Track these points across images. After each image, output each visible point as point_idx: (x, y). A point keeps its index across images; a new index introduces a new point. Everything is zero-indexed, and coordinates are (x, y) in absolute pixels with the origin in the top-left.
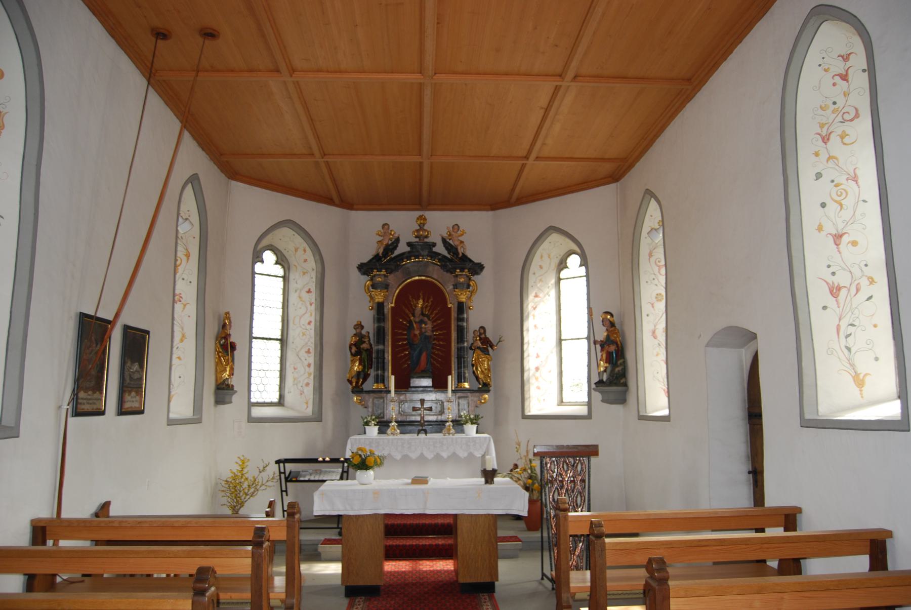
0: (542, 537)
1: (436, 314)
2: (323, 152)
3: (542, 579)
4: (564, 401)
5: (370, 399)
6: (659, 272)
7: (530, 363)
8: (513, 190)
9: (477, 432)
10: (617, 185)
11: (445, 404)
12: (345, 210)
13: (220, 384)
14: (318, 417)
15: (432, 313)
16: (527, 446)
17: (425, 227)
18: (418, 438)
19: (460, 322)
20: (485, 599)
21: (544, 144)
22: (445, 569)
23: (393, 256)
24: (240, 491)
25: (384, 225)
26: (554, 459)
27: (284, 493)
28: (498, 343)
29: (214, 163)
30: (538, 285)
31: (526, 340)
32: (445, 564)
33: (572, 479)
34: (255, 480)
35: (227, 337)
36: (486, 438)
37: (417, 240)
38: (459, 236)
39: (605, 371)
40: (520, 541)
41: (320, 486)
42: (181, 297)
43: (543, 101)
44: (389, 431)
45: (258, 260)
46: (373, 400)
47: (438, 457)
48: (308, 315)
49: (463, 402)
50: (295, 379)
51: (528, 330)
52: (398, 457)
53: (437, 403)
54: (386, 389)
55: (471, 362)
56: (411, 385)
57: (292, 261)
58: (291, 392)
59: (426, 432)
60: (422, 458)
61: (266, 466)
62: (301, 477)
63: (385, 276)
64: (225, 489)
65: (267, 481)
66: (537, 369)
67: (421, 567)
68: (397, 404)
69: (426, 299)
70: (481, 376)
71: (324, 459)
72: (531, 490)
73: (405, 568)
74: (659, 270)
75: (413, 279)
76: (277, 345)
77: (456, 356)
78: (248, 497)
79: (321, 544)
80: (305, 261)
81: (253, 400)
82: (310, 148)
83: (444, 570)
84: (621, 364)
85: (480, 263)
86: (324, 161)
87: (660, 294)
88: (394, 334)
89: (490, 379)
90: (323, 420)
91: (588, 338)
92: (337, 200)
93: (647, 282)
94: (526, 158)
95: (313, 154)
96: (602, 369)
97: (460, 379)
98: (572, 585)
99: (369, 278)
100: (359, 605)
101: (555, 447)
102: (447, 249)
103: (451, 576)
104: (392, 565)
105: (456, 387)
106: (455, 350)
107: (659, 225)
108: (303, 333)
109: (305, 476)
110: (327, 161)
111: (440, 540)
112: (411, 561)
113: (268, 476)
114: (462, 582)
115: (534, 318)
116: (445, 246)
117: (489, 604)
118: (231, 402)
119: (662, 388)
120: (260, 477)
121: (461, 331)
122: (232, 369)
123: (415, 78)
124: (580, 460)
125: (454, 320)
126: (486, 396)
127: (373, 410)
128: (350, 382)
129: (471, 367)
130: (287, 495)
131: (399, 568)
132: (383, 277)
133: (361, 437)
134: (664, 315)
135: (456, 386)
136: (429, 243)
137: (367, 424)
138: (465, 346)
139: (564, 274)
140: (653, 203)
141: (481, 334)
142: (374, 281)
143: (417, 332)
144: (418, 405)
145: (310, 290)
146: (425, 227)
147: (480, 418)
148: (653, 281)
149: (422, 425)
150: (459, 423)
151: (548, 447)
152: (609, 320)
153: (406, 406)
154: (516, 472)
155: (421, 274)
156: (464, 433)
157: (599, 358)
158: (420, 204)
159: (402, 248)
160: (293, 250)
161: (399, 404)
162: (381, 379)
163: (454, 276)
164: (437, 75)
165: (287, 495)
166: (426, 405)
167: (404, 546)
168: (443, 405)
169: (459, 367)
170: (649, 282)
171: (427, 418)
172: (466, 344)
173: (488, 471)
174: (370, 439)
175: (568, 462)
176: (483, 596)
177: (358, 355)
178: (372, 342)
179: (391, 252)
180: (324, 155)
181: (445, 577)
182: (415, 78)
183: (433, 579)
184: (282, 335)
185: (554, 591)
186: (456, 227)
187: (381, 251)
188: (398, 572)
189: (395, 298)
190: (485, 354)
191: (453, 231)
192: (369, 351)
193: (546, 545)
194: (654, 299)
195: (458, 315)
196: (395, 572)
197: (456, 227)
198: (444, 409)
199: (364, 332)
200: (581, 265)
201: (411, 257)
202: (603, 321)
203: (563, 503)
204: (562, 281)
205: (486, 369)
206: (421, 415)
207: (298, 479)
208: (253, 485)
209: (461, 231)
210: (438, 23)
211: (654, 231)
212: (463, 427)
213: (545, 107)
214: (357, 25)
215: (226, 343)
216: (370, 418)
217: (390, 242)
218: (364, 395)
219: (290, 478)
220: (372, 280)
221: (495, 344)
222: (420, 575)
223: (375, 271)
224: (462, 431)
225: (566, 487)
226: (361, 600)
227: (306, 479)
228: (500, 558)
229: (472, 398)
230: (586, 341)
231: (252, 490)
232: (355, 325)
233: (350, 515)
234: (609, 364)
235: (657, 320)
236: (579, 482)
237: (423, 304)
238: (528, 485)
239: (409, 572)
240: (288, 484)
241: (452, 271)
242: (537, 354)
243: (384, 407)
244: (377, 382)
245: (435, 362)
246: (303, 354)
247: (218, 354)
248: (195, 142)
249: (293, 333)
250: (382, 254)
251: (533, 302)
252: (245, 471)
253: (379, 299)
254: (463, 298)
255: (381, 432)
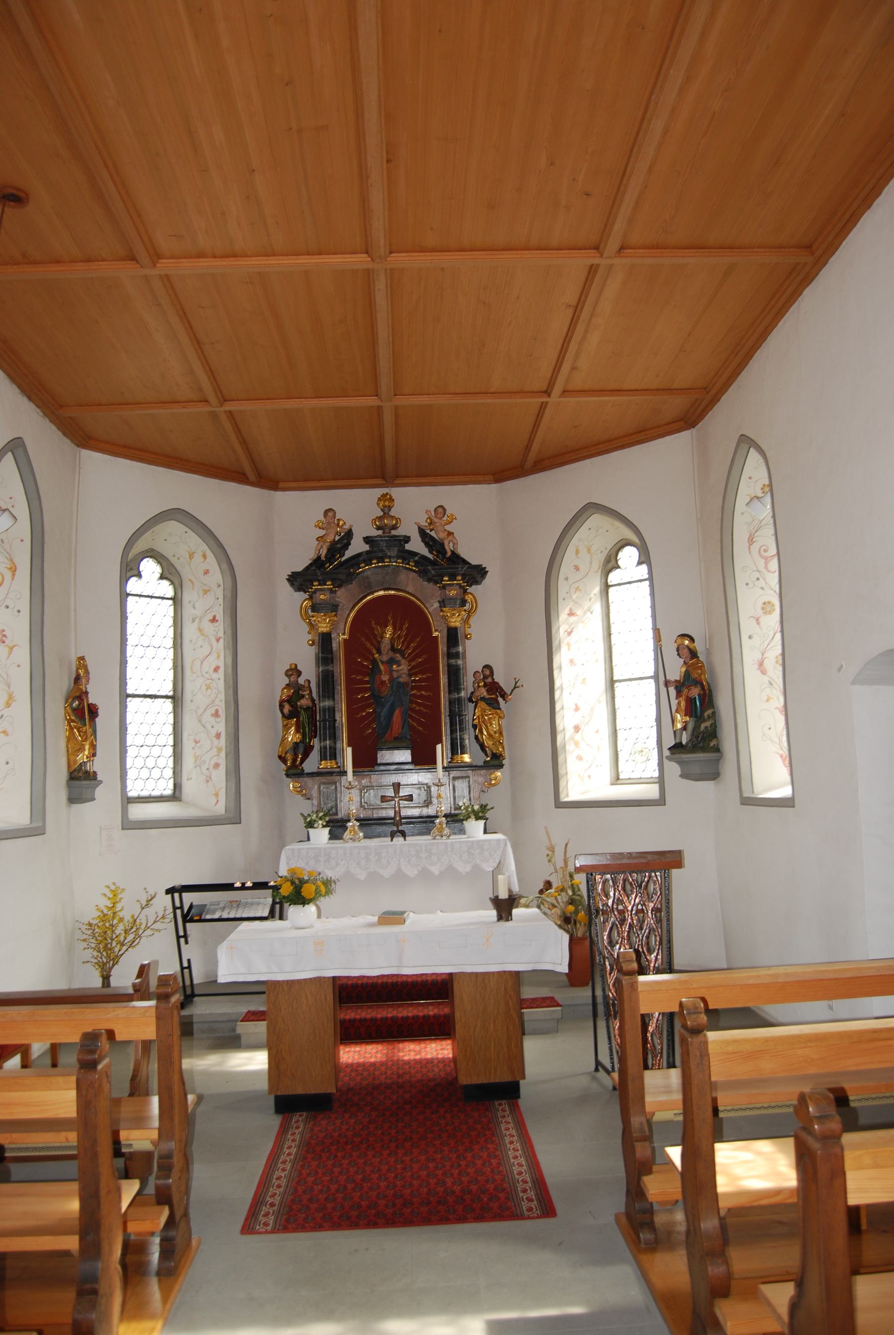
0: (594, 997)
1: (415, 648)
2: (223, 396)
3: (597, 1070)
4: (621, 777)
5: (314, 786)
6: (766, 567)
7: (566, 720)
8: (528, 448)
9: (485, 832)
10: (692, 434)
11: (432, 789)
12: (266, 492)
13: (75, 770)
14: (234, 817)
15: (407, 648)
16: (565, 852)
17: (392, 513)
18: (392, 845)
19: (453, 658)
20: (504, 1111)
21: (574, 368)
22: (440, 1056)
23: (343, 559)
24: (112, 939)
25: (326, 512)
26: (608, 876)
27: (182, 940)
28: (512, 691)
29: (51, 421)
30: (574, 597)
31: (557, 684)
32: (439, 1047)
33: (640, 907)
34: (135, 921)
35: (82, 695)
36: (499, 840)
37: (380, 532)
38: (446, 524)
39: (684, 728)
40: (558, 1005)
41: (230, 933)
42: (5, 636)
43: (570, 295)
44: (347, 835)
45: (129, 574)
46: (319, 788)
47: (425, 875)
48: (214, 656)
49: (462, 785)
50: (196, 758)
51: (560, 668)
52: (362, 875)
53: (420, 788)
54: (339, 770)
55: (471, 721)
56: (379, 761)
57: (185, 572)
58: (191, 779)
59: (403, 834)
60: (399, 877)
61: (151, 899)
62: (207, 914)
63: (331, 591)
64: (87, 937)
65: (155, 922)
66: (577, 729)
67: (401, 1054)
68: (358, 792)
69: (398, 626)
70: (488, 743)
71: (243, 884)
72: (573, 921)
73: (376, 1057)
74: (766, 564)
75: (376, 594)
76: (168, 705)
77: (448, 714)
78: (125, 948)
79: (242, 1021)
80: (206, 572)
81: (132, 794)
82: (201, 390)
83: (437, 1058)
84: (709, 717)
85: (481, 565)
86: (225, 411)
87: (769, 603)
88: (349, 682)
89: (503, 748)
90: (242, 821)
91: (656, 677)
92: (252, 477)
93: (747, 584)
94: (547, 393)
95: (206, 401)
96: (679, 726)
97: (456, 748)
98: (648, 1099)
99: (306, 596)
100: (297, 1128)
101: (609, 857)
102: (427, 544)
103: (448, 1069)
104: (355, 1052)
105: (450, 762)
106: (445, 705)
107: (763, 493)
108: (206, 685)
109: (214, 912)
110: (230, 412)
111: (431, 1008)
112: (385, 1044)
113: (156, 913)
114: (465, 1083)
115: (569, 649)
116: (423, 541)
117: (510, 1119)
118: (93, 799)
119: (777, 753)
120: (142, 916)
121: (455, 675)
122: (93, 747)
123: (359, 261)
124: (650, 877)
125: (443, 657)
126: (499, 774)
127: (319, 803)
128: (282, 759)
129: (472, 730)
130: (187, 942)
131: (365, 1057)
132: (328, 593)
133: (301, 847)
134: (779, 635)
135: (450, 760)
136: (398, 536)
137: (310, 825)
138: (461, 697)
139: (613, 578)
140: (753, 454)
141: (485, 677)
142: (314, 600)
143: (385, 678)
144: (390, 793)
145: (214, 617)
146: (392, 513)
147: (488, 810)
148: (757, 583)
149: (397, 824)
150: (455, 818)
151: (597, 857)
152: (687, 646)
153: (372, 795)
154: (550, 893)
155: (387, 586)
156: (465, 834)
157: (674, 708)
158: (383, 478)
159: (357, 546)
160: (187, 556)
161: (361, 792)
162: (331, 754)
163: (439, 587)
164: (393, 255)
165: (187, 942)
166: (403, 792)
167: (373, 1021)
168: (430, 791)
169: (453, 731)
170: (751, 585)
171: (405, 812)
172: (463, 694)
173: (502, 900)
174: (315, 848)
175: (631, 880)
176: (500, 1105)
177: (294, 718)
178: (315, 695)
179: (339, 553)
180: (224, 400)
181: (440, 1071)
182: (359, 261)
183: (419, 1076)
184: (175, 689)
185: (617, 1093)
186: (441, 510)
187: (324, 552)
188: (363, 1064)
189: (348, 625)
190: (494, 708)
191: (436, 517)
192: (311, 711)
193: (601, 1009)
194: (761, 612)
195: (448, 648)
196: (358, 1064)
197: (440, 510)
198: (431, 797)
199: (301, 681)
200: (640, 563)
201: (371, 560)
202: (678, 650)
203: (628, 961)
204: (611, 590)
205: (495, 732)
206: (395, 808)
207: (203, 917)
208: (132, 928)
209: (448, 517)
210: (388, 161)
211: (755, 499)
212: (463, 824)
213: (575, 304)
214: (254, 171)
215: (81, 706)
216: (315, 815)
217: (337, 538)
218: (305, 779)
219: (190, 916)
220: (311, 598)
221: (508, 691)
222: (398, 1068)
223: (316, 583)
224: (462, 831)
225: (629, 920)
226: (301, 1120)
227: (216, 916)
228: (528, 1034)
229: (477, 778)
230: (652, 681)
231: (130, 937)
232: (287, 671)
233: (278, 981)
234: (691, 716)
235: (766, 645)
236: (650, 912)
237: (394, 633)
238: (568, 915)
239: (382, 1063)
240: (188, 925)
241: (435, 580)
242: (576, 705)
243: (336, 798)
244: (323, 757)
245: (415, 724)
246: (208, 717)
247: (69, 723)
248: (14, 386)
249: (191, 686)
250: (326, 557)
251: (567, 624)
252: (119, 907)
253: (324, 628)
254: (455, 621)
255: (333, 836)
